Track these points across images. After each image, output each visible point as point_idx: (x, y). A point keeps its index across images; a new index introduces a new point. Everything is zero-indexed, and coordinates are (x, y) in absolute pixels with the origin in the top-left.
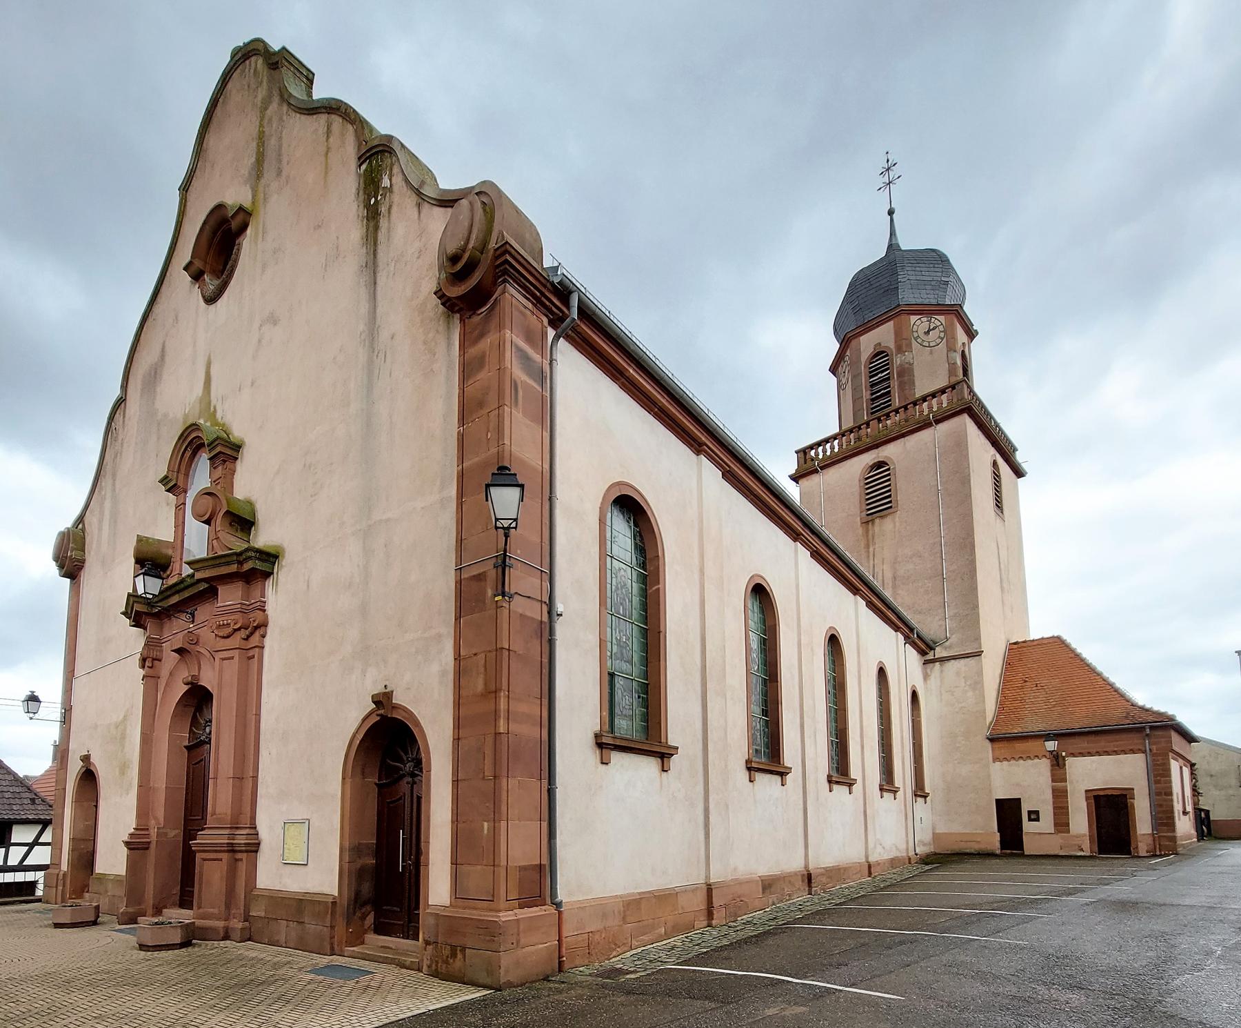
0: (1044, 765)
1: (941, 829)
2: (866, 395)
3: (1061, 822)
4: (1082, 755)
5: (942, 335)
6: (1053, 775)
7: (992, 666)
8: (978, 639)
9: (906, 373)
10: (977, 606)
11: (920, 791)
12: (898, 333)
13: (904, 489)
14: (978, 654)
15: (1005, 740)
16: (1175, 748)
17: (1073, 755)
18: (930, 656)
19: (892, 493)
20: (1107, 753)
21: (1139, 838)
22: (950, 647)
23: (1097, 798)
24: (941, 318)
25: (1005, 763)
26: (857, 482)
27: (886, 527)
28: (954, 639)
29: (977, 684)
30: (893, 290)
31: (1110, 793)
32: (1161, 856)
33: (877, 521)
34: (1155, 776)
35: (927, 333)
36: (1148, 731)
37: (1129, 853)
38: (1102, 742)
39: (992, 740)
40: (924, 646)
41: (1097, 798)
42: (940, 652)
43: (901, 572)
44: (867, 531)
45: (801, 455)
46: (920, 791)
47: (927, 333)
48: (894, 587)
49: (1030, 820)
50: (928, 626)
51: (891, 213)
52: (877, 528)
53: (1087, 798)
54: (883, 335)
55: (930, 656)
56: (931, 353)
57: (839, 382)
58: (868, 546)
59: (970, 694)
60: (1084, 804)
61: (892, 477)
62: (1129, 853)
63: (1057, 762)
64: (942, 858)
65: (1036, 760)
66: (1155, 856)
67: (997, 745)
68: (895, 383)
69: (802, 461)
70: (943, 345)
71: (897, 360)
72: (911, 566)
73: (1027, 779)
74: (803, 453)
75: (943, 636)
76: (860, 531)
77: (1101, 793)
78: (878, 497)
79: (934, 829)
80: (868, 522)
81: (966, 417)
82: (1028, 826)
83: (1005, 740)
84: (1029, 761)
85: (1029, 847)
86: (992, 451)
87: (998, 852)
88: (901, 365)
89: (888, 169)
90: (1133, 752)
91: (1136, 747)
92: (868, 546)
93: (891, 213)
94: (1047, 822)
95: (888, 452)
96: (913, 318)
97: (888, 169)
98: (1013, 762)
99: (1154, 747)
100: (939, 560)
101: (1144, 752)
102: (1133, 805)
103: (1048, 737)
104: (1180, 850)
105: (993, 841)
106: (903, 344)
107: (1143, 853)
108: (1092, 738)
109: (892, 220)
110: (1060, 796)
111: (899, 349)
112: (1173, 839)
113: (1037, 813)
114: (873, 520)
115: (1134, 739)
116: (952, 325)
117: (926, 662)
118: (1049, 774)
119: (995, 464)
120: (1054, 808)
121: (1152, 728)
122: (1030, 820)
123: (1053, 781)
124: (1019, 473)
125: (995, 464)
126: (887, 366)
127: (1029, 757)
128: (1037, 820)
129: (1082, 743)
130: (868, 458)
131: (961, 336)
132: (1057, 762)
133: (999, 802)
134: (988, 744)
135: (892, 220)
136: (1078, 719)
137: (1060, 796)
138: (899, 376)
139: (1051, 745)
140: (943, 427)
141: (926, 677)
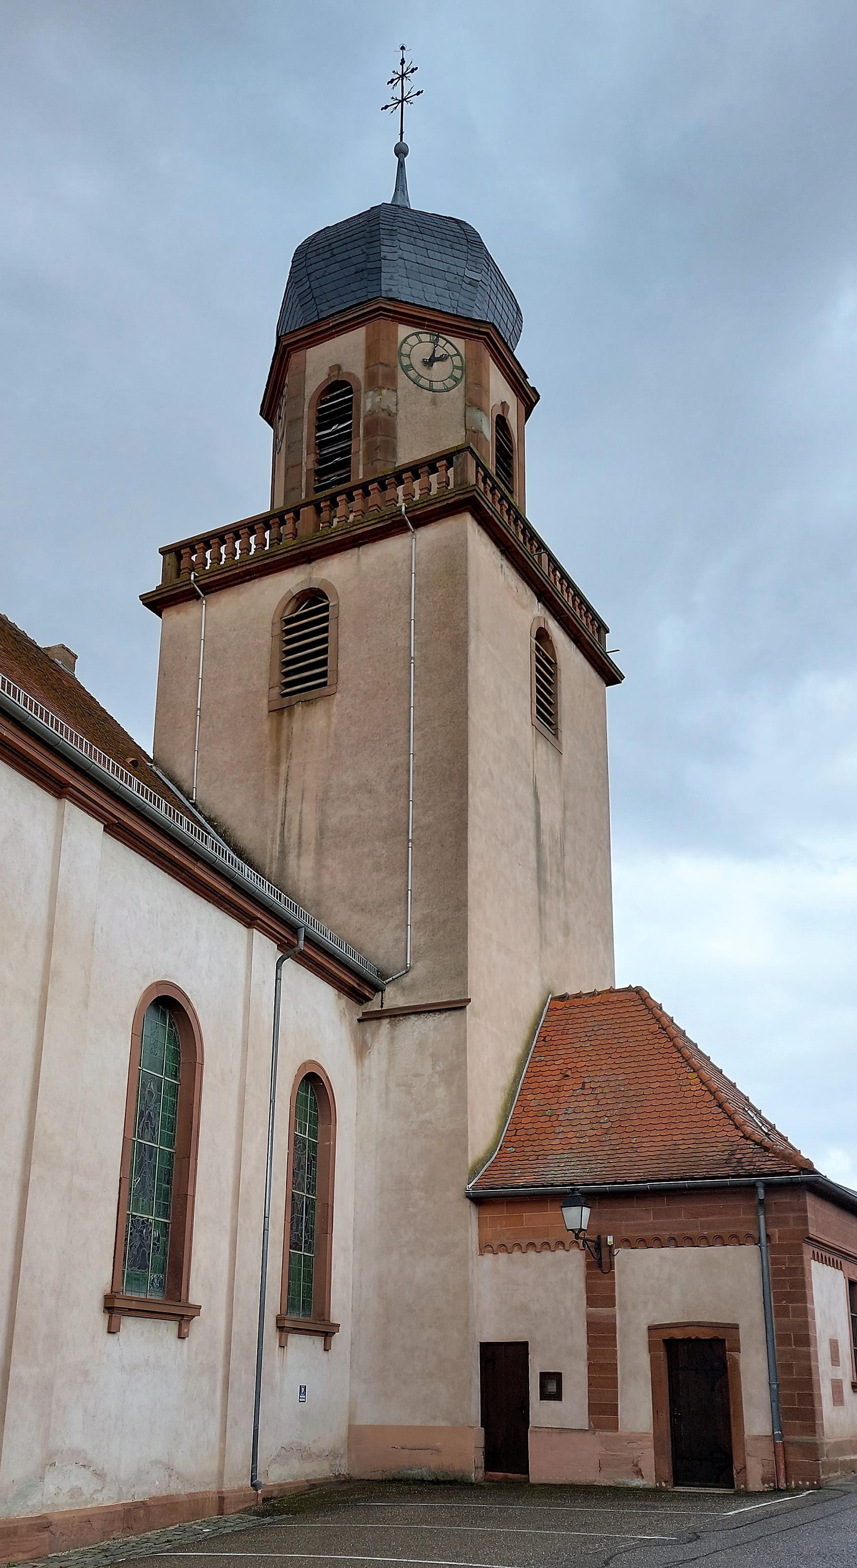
0: (573, 1263)
1: (368, 1417)
2: (308, 461)
3: (603, 1409)
4: (645, 1243)
5: (458, 374)
6: (589, 1289)
7: (494, 1045)
8: (461, 972)
9: (383, 428)
10: (466, 905)
11: (305, 1306)
12: (372, 351)
13: (352, 651)
14: (458, 1006)
15: (504, 1201)
16: (813, 1232)
17: (628, 1243)
18: (374, 1006)
19: (329, 656)
20: (691, 1241)
21: (749, 1447)
22: (412, 988)
23: (671, 1345)
24: (460, 343)
25: (503, 1256)
26: (268, 625)
27: (316, 722)
28: (419, 970)
29: (455, 1072)
30: (372, 271)
31: (693, 1333)
32: (788, 1491)
33: (298, 709)
34: (778, 1297)
35: (429, 363)
36: (761, 1192)
37: (730, 1484)
38: (681, 1216)
39: (479, 1200)
40: (357, 985)
41: (671, 1345)
42: (393, 998)
43: (333, 821)
44: (279, 730)
45: (171, 558)
46: (305, 1306)
47: (429, 363)
48: (320, 850)
49: (545, 1396)
50: (373, 939)
51: (401, 151)
52: (296, 725)
53: (652, 1347)
54: (345, 351)
55: (374, 1006)
56: (434, 402)
57: (276, 436)
58: (277, 760)
59: (441, 1092)
60: (643, 1360)
61: (331, 624)
62: (730, 1484)
63: (599, 1261)
64: (358, 1492)
65: (560, 1253)
66: (777, 1492)
67: (491, 1213)
68: (359, 445)
69: (172, 571)
70: (458, 393)
71: (367, 402)
72: (352, 811)
73: (529, 1293)
74: (175, 554)
75: (399, 965)
76: (266, 727)
77: (678, 1334)
78: (305, 655)
79: (352, 1415)
80: (279, 712)
81: (468, 524)
82: (540, 1412)
83: (504, 1201)
84: (548, 1255)
85: (543, 1465)
86: (538, 610)
87: (476, 1474)
88: (372, 412)
89: (403, 76)
90: (737, 1239)
91: (743, 1230)
92: (277, 760)
93: (401, 151)
94: (573, 1407)
95: (333, 572)
96: (403, 331)
97: (403, 76)
98: (517, 1254)
99: (776, 1232)
100: (402, 802)
101: (758, 1242)
102: (736, 1363)
103: (569, 1197)
104: (835, 1477)
105: (466, 1452)
106: (381, 374)
107: (755, 1484)
108: (663, 1205)
109: (401, 165)
110: (601, 1336)
111: (372, 381)
112: (812, 1450)
113: (557, 1377)
114: (290, 707)
115: (736, 1214)
116: (479, 361)
117: (367, 1018)
118: (582, 1285)
119: (542, 636)
120: (590, 1366)
121: (770, 1187)
122: (545, 1396)
123: (591, 1301)
124: (610, 675)
125: (542, 636)
126: (344, 413)
127: (546, 1245)
128: (557, 1396)
129: (643, 1217)
130: (291, 581)
131: (499, 390)
132: (599, 1261)
133: (485, 1347)
134: (471, 1213)
135: (401, 165)
136: (643, 1159)
137: (601, 1336)
138: (366, 429)
139: (578, 1217)
140: (430, 534)
141: (362, 1050)
